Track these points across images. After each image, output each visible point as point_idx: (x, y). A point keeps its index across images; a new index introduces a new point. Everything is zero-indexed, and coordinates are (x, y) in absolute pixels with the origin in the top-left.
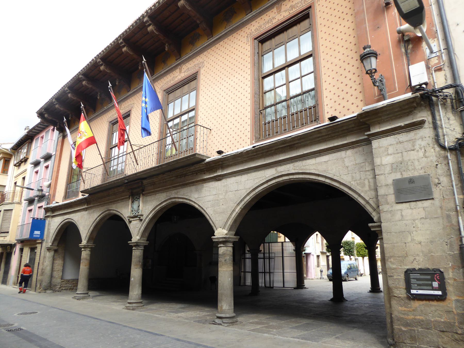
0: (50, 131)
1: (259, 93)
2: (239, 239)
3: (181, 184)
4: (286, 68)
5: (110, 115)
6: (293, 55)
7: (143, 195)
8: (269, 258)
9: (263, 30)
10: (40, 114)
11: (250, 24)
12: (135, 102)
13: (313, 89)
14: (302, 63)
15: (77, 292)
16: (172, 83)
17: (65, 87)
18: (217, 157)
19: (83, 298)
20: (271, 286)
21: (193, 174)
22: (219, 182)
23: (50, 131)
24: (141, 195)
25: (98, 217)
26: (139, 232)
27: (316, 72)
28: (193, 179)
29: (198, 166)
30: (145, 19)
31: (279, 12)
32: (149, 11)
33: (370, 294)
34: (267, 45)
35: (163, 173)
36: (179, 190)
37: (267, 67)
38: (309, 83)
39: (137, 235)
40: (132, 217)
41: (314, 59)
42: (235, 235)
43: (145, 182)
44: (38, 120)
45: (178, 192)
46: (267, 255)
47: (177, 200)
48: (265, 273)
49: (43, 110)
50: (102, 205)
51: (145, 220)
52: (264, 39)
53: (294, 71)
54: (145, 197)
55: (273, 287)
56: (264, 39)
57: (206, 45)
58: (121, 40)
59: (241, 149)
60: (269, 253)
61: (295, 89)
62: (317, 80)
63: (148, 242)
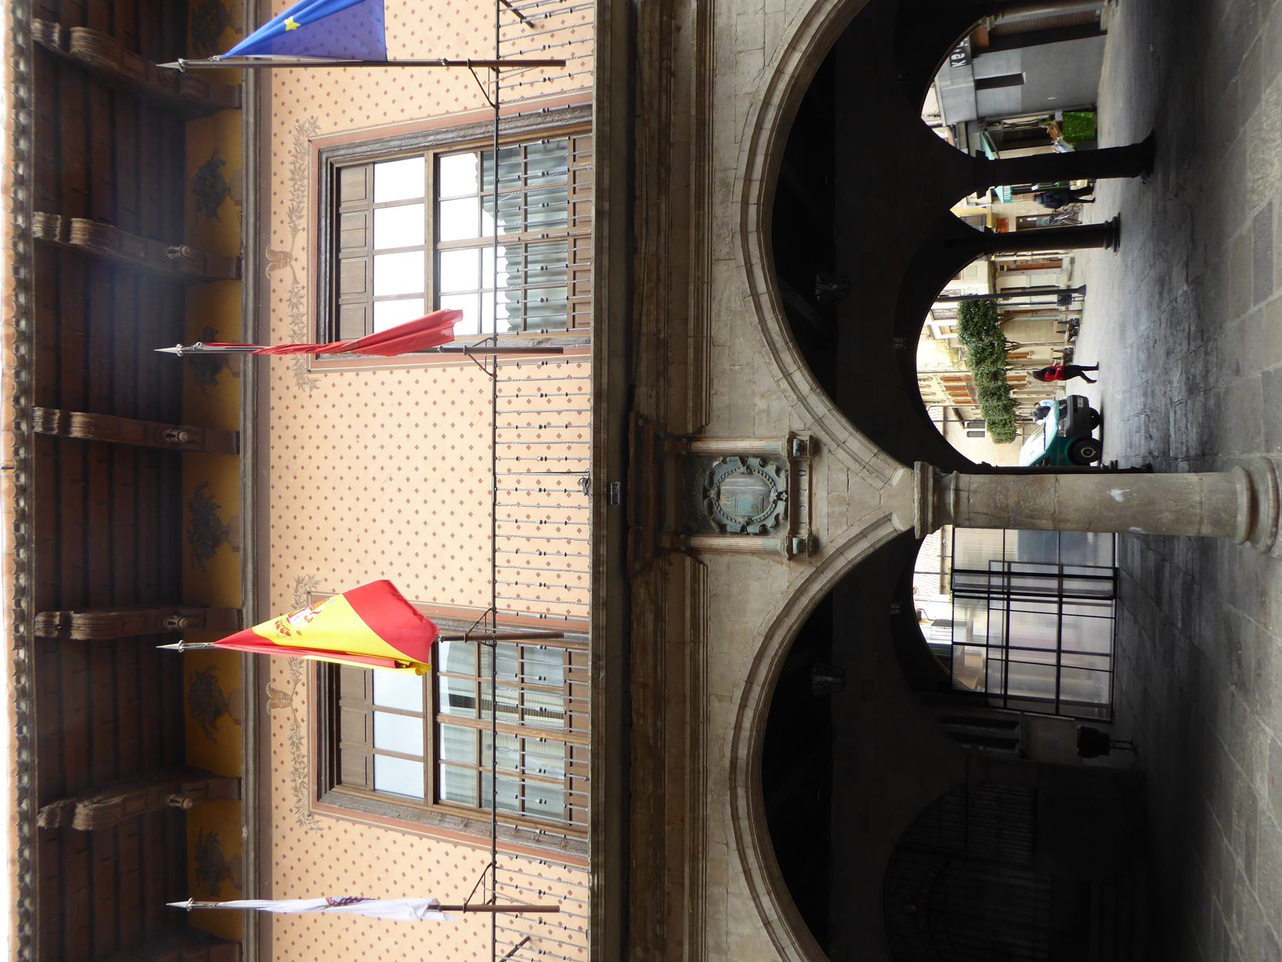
3: (693, 149)
4: (439, 719)
5: (291, 801)
7: (700, 432)
8: (1009, 574)
11: (274, 941)
12: (296, 571)
16: (307, 747)
20: (1109, 573)
21: (668, 92)
24: (700, 446)
25: (755, 897)
28: (688, 95)
29: (647, 36)
30: (37, 230)
31: (286, 258)
32: (23, 144)
33: (1121, 249)
34: (351, 765)
35: (632, 250)
36: (718, 176)
40: (794, 531)
43: (645, 404)
45: (725, 184)
46: (996, 581)
47: (745, 734)
48: (1061, 576)
49: (36, 25)
50: (697, 853)
51: (819, 421)
52: (331, 770)
55: (1115, 570)
56: (331, 770)
57: (251, 120)
58: (38, 412)
60: (990, 573)
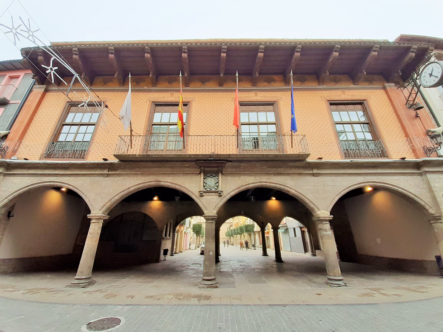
0: (7, 77)
1: (58, 132)
2: (333, 218)
6: (346, 119)
9: (159, 100)
10: (26, 52)
13: (88, 142)
14: (72, 126)
15: (76, 277)
17: (299, 44)
18: (103, 161)
19: (91, 283)
22: (316, 177)
23: (7, 77)
26: (216, 207)
27: (94, 134)
37: (68, 121)
38: (88, 138)
39: (214, 209)
40: (204, 192)
41: (95, 127)
42: (108, 215)
44: (20, 57)
51: (225, 197)
53: (83, 128)
54: (224, 177)
59: (96, 161)
61: (79, 138)
62: (92, 138)
63: (109, 216)
